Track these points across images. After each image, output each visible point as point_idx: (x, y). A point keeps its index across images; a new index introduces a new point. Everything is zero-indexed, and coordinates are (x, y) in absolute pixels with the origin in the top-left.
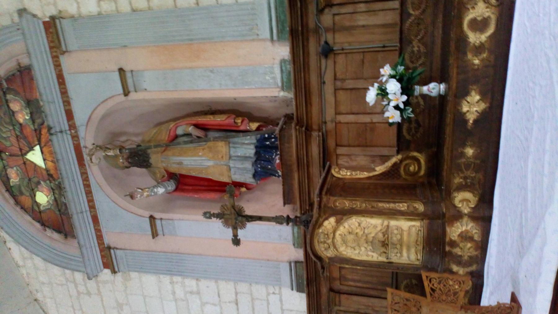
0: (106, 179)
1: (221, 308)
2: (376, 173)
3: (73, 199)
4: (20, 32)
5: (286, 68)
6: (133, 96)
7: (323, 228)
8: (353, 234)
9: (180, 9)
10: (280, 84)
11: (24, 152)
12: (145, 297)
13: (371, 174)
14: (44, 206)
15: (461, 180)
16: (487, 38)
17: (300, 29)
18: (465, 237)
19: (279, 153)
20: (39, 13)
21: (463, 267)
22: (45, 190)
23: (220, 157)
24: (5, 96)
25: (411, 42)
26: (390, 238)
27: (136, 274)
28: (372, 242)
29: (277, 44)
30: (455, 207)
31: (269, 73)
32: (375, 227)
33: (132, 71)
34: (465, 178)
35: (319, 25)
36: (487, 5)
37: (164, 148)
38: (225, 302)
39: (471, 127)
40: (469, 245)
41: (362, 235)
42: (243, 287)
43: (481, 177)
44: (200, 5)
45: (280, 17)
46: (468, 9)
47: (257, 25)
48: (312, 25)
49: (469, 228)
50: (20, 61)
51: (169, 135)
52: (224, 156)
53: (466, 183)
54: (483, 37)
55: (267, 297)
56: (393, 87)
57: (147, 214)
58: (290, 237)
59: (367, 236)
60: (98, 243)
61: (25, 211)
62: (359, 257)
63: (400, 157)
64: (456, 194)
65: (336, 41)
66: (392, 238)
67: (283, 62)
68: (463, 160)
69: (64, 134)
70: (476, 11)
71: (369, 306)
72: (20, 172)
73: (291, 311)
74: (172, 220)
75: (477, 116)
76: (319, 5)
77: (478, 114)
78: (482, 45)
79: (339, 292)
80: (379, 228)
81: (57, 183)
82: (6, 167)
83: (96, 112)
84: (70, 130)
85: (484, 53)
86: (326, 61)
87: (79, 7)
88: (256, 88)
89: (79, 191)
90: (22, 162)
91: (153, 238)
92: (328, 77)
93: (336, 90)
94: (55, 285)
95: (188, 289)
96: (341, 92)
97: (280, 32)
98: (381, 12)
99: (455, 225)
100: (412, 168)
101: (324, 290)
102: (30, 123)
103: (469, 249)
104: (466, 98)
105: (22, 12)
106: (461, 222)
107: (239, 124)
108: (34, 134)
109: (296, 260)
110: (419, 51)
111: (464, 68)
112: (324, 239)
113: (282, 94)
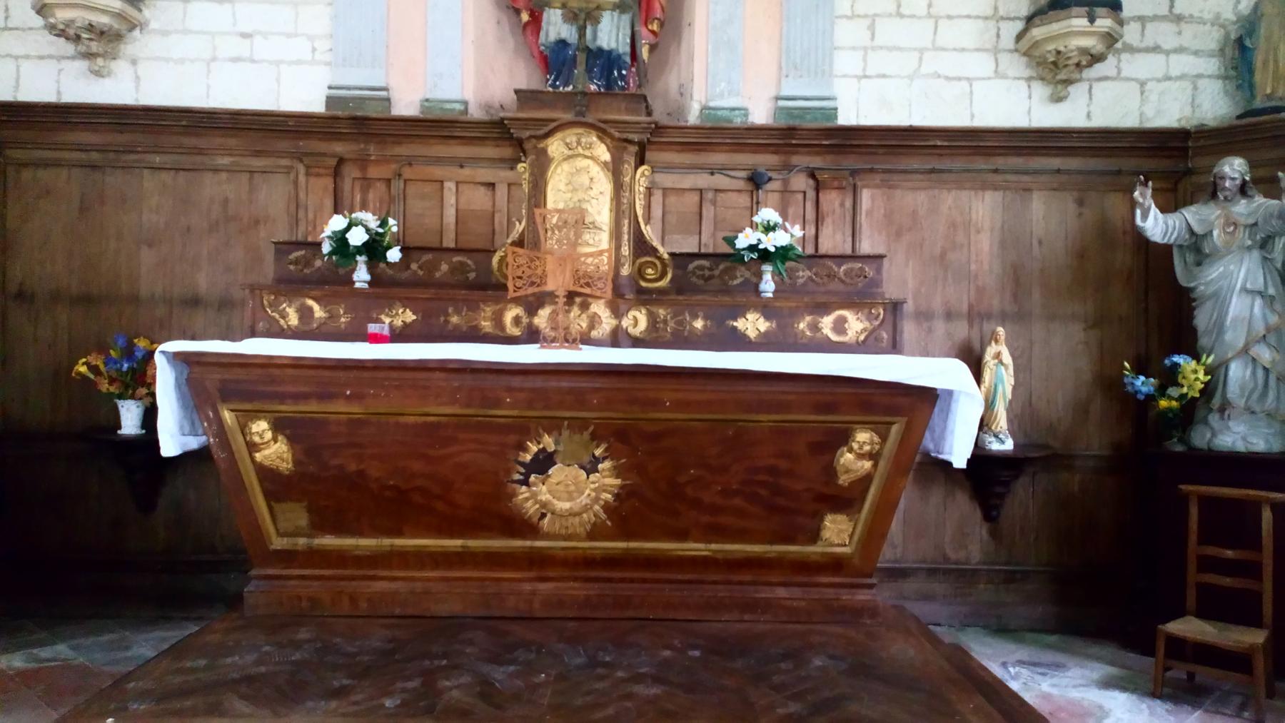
2: (643, 226)
5: (737, 116)
7: (599, 142)
8: (590, 183)
10: (712, 104)
13: (641, 220)
16: (826, 335)
17: (794, 142)
18: (594, 321)
19: (602, 90)
25: (810, 269)
26: (589, 230)
31: (729, 88)
32: (599, 213)
34: (665, 322)
35: (795, 171)
36: (859, 331)
39: (728, 325)
40: (584, 325)
41: (590, 195)
43: (665, 339)
45: (809, 113)
46: (857, 314)
47: (801, 76)
49: (604, 325)
53: (658, 323)
55: (303, 35)
59: (588, 201)
62: (552, 190)
63: (666, 256)
64: (644, 311)
65: (770, 195)
67: (745, 111)
73: (278, 81)
75: (740, 330)
76: (822, 172)
77: (743, 330)
79: (337, 173)
85: (811, 333)
86: (744, 178)
92: (720, 181)
93: (701, 190)
96: (696, 198)
99: (607, 310)
100: (650, 271)
101: (339, 148)
103: (579, 324)
104: (762, 317)
107: (650, 27)
109: (392, 100)
110: (798, 277)
111: (796, 314)
112: (585, 143)
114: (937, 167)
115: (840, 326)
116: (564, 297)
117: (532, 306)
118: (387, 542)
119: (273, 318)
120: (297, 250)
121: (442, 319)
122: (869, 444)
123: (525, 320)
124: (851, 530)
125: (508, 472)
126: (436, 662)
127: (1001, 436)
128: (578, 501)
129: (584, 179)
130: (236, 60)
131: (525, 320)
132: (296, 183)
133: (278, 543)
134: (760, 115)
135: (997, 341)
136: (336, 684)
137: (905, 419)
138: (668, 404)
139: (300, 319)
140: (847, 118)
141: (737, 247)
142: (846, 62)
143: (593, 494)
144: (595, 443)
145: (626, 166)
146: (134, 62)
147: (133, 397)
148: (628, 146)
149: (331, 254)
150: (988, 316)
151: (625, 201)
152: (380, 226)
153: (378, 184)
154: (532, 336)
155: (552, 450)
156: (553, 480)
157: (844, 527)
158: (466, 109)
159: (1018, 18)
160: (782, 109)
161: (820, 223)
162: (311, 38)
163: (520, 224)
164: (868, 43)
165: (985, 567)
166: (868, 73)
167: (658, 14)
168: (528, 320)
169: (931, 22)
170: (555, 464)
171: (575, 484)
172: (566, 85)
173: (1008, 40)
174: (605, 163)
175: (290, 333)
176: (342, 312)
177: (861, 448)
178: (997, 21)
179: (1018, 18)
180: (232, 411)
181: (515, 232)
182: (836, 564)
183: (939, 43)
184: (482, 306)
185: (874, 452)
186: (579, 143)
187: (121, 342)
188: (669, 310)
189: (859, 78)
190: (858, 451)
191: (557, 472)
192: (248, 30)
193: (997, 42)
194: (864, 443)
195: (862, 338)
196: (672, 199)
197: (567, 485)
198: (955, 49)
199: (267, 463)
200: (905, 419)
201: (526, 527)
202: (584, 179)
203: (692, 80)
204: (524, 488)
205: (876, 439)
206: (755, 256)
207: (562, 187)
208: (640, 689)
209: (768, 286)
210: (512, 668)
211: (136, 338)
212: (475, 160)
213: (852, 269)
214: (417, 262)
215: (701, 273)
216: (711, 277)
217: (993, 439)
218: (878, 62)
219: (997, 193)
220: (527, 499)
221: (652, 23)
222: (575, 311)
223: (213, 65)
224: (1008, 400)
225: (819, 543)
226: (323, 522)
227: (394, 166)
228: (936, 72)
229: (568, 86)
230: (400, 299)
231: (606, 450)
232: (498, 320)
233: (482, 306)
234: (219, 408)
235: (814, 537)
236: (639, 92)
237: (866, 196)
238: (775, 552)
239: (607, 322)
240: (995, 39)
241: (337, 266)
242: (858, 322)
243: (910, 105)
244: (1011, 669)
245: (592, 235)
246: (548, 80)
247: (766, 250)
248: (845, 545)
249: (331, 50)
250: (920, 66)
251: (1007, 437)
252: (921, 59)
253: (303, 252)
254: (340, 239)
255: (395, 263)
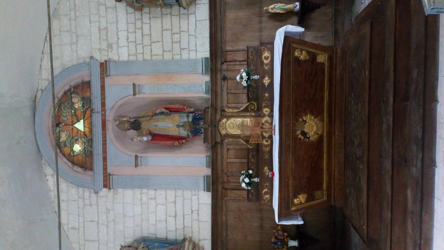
0: (115, 136)
1: (166, 206)
3: (96, 147)
4: (88, 66)
5: (208, 84)
6: (137, 96)
7: (222, 121)
9: (165, 60)
10: (205, 91)
11: (74, 123)
12: (124, 204)
13: (239, 110)
14: (77, 153)
15: (265, 104)
17: (214, 69)
18: (267, 122)
20: (99, 59)
21: (267, 133)
22: (80, 143)
23: (176, 122)
24: (71, 95)
25: (251, 66)
27: (122, 189)
28: (238, 126)
29: (204, 76)
30: (264, 113)
32: (239, 121)
33: (139, 85)
34: (266, 104)
35: (222, 68)
37: (151, 117)
38: (169, 203)
40: (268, 124)
42: (179, 193)
43: (271, 103)
44: (174, 59)
47: (197, 68)
48: (219, 68)
49: (268, 119)
50: (84, 79)
51: (153, 112)
52: (178, 121)
54: (268, 61)
55: (191, 197)
56: (244, 74)
57: (134, 154)
58: (205, 163)
59: (236, 124)
60: (103, 173)
61: (64, 156)
65: (228, 75)
66: (244, 123)
68: (265, 98)
69: (99, 114)
70: (265, 54)
71: (241, 195)
72: (68, 134)
73: (203, 204)
74: (147, 157)
76: (222, 61)
78: (267, 64)
79: (226, 189)
80: (241, 121)
81: (88, 139)
82: (60, 132)
83: (117, 103)
84: (102, 112)
87: (119, 57)
88: (194, 93)
89: (100, 144)
90: (72, 128)
91: (136, 167)
92: (225, 88)
93: (227, 93)
94: (70, 201)
95: (150, 197)
96: (229, 95)
97: (206, 70)
98: (244, 65)
100: (252, 108)
101: (220, 189)
102: (81, 109)
103: (268, 126)
105: (91, 58)
106: (265, 117)
107: (186, 108)
108: (82, 113)
110: (253, 69)
111: (263, 70)
113: (205, 95)
114: (220, 29)
115: (266, 58)
116: (262, 129)
117: (264, 137)
118: (325, 172)
119: (267, 201)
120: (249, 196)
121: (267, 160)
122: (298, 52)
123: (267, 139)
124: (321, 55)
125: (306, 142)
126: (354, 158)
127: (295, 6)
128: (314, 125)
129: (231, 125)
130: (198, 215)
131: (267, 139)
132: (229, 200)
133: (325, 198)
134: (207, 78)
135: (268, 9)
136: (358, 180)
137: (292, 44)
138: (288, 103)
139: (268, 194)
140: (207, 55)
141: (246, 86)
142: (193, 56)
143: (312, 121)
144: (298, 121)
145: (227, 115)
146: (200, 240)
147: (288, 242)
148: (222, 114)
149: (251, 187)
150: (261, 11)
151: (236, 114)
152: (244, 175)
153: (228, 179)
154: (271, 137)
155: (301, 132)
156: (308, 131)
157: (320, 57)
158: (208, 156)
159: (180, 9)
160: (205, 72)
161: (235, 61)
162: (192, 195)
163: (241, 141)
164: (188, 50)
165: (334, 7)
166: (195, 49)
167: (182, 106)
168: (267, 138)
169: (182, 33)
170: (304, 131)
171: (309, 126)
172: (201, 130)
173: (185, 11)
174: (227, 120)
175: (271, 197)
176: (266, 184)
177: (299, 54)
178: (181, 14)
179: (180, 9)
180: (292, 207)
181: (243, 142)
182: (330, 58)
183: (187, 30)
184: (263, 150)
185: (300, 50)
186: (222, 126)
187: (273, 245)
188: (263, 103)
189: (197, 52)
190: (300, 55)
191: (306, 130)
192: (191, 211)
193: (186, 14)
194: (298, 53)
195: (270, 52)
196: (230, 101)
197: (310, 128)
198: (188, 26)
199: (305, 200)
200: (292, 44)
201: (321, 138)
202: (231, 125)
203: (199, 97)
204: (310, 138)
205: (297, 50)
206: (249, 81)
207: (233, 130)
208: (359, 109)
209: (256, 77)
210: (355, 140)
211: (272, 242)
212: (222, 154)
213: (251, 54)
214: (251, 167)
215: (252, 94)
216: (253, 91)
217: (296, 8)
218: (192, 47)
219: (226, 12)
220: (313, 138)
221: (185, 108)
222: (264, 127)
223: (200, 220)
224: (285, 5)
225: (325, 63)
226: (320, 187)
227: (224, 175)
228: (194, 31)
229: (202, 130)
230: (262, 170)
231: (300, 118)
232: (267, 146)
233: (263, 150)
234: (291, 210)
235: (323, 64)
236: (203, 111)
237: (228, 48)
238: (327, 74)
239: (267, 118)
240: (185, 15)
241: (253, 186)
242: (266, 53)
243: (203, 37)
244: (363, 2)
245: (245, 123)
246: (199, 135)
247: (247, 79)
248: (325, 56)
249: (195, 190)
250: (193, 35)
251: (295, 4)
252: (191, 35)
253: (250, 195)
254: (247, 184)
255: (253, 171)
